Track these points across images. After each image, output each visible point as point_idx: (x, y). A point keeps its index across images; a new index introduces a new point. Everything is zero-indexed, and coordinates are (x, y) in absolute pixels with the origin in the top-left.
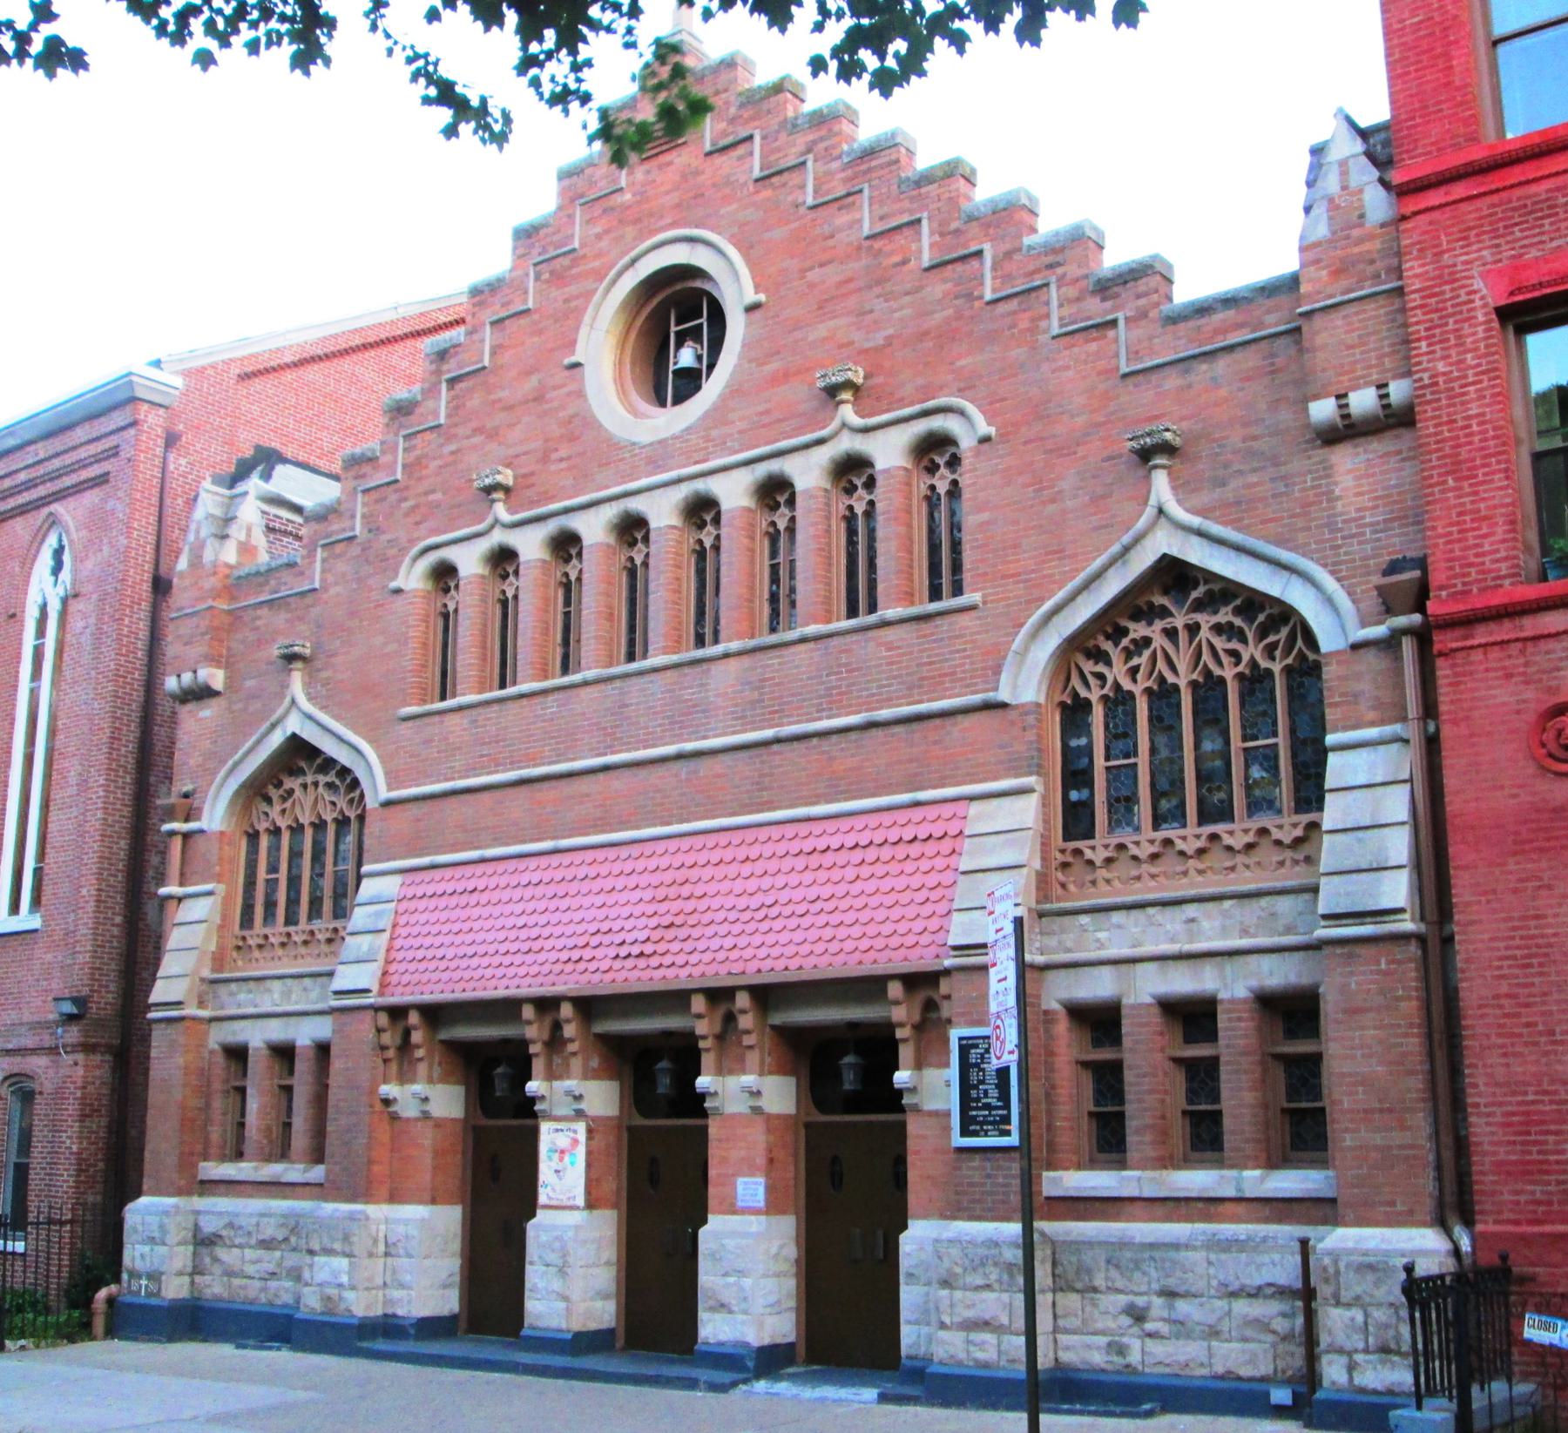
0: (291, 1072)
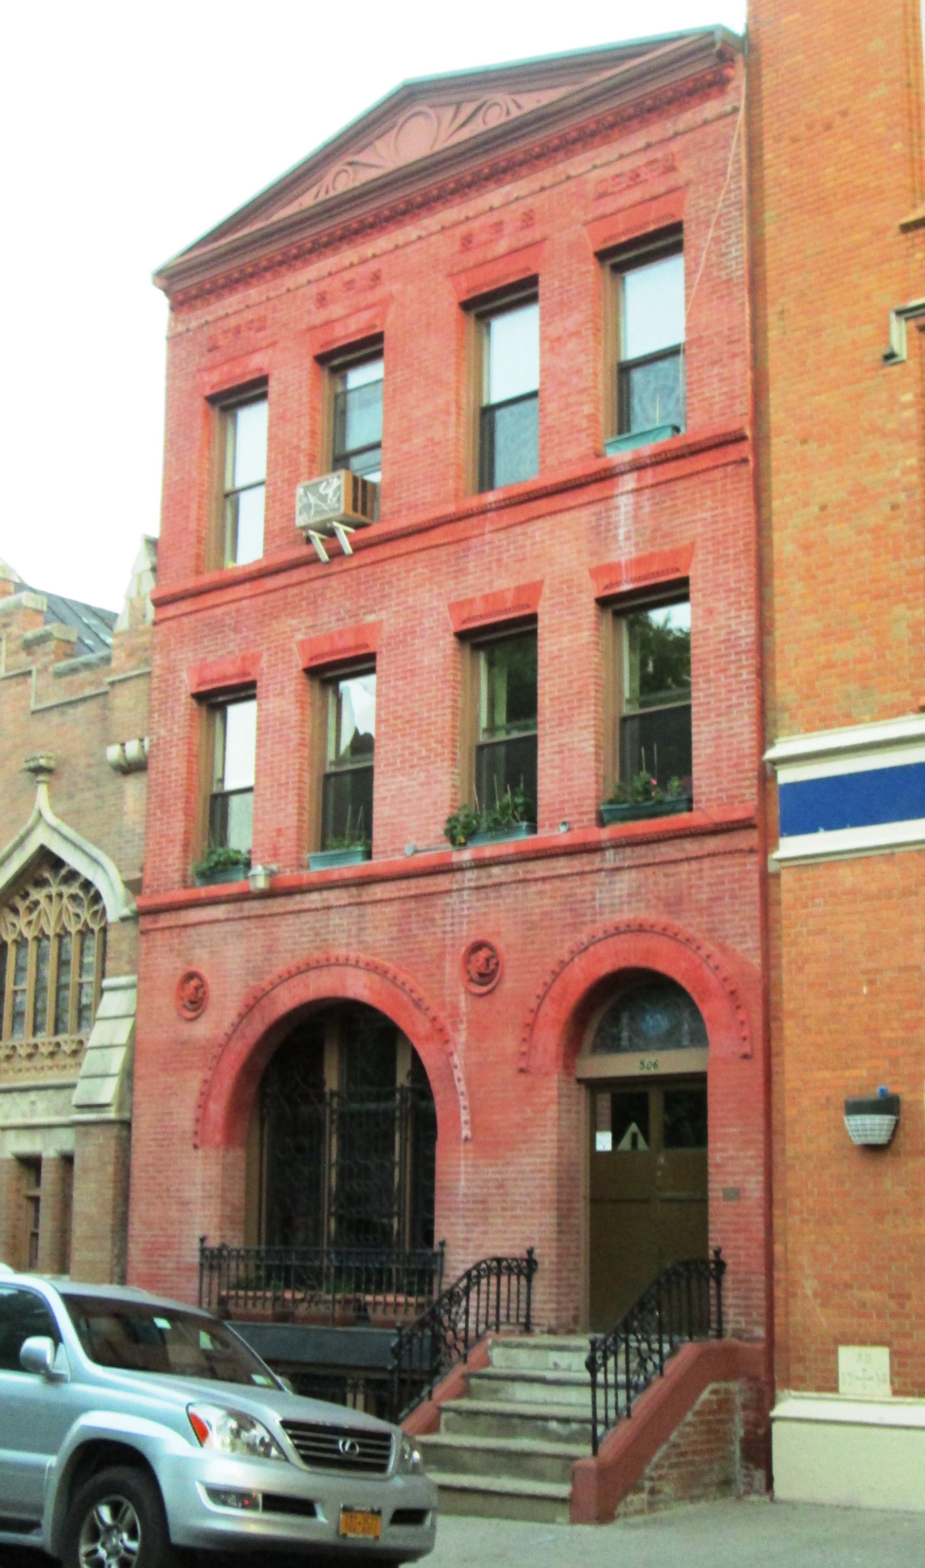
0: (38, 1182)
